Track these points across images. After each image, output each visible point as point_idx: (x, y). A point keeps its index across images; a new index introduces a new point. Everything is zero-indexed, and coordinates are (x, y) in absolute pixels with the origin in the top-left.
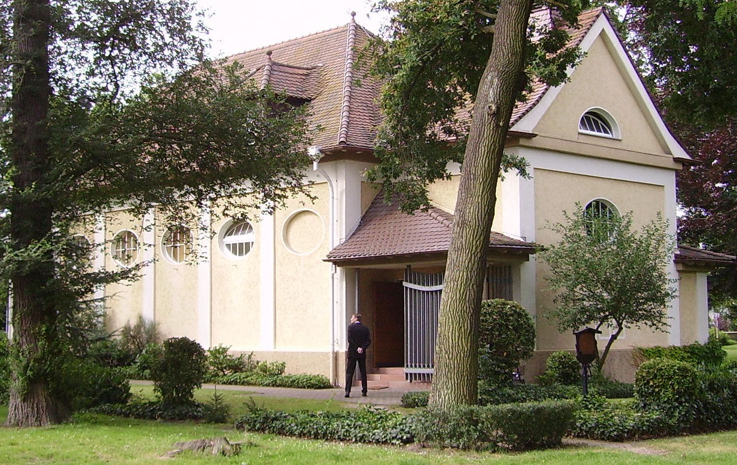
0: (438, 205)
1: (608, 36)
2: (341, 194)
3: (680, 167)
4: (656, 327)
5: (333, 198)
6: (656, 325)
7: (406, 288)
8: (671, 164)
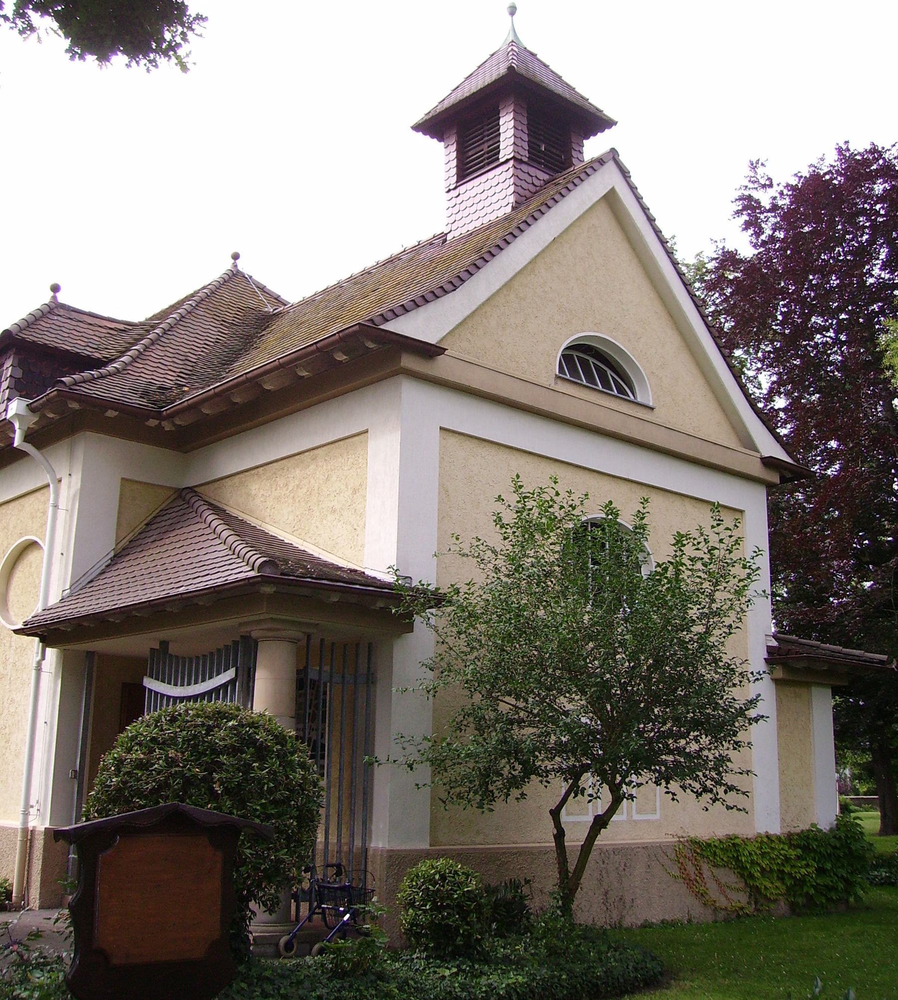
0: (260, 523)
1: (623, 205)
2: (74, 500)
3: (775, 478)
4: (710, 795)
5: (56, 506)
6: (711, 791)
7: (150, 691)
8: (757, 470)
